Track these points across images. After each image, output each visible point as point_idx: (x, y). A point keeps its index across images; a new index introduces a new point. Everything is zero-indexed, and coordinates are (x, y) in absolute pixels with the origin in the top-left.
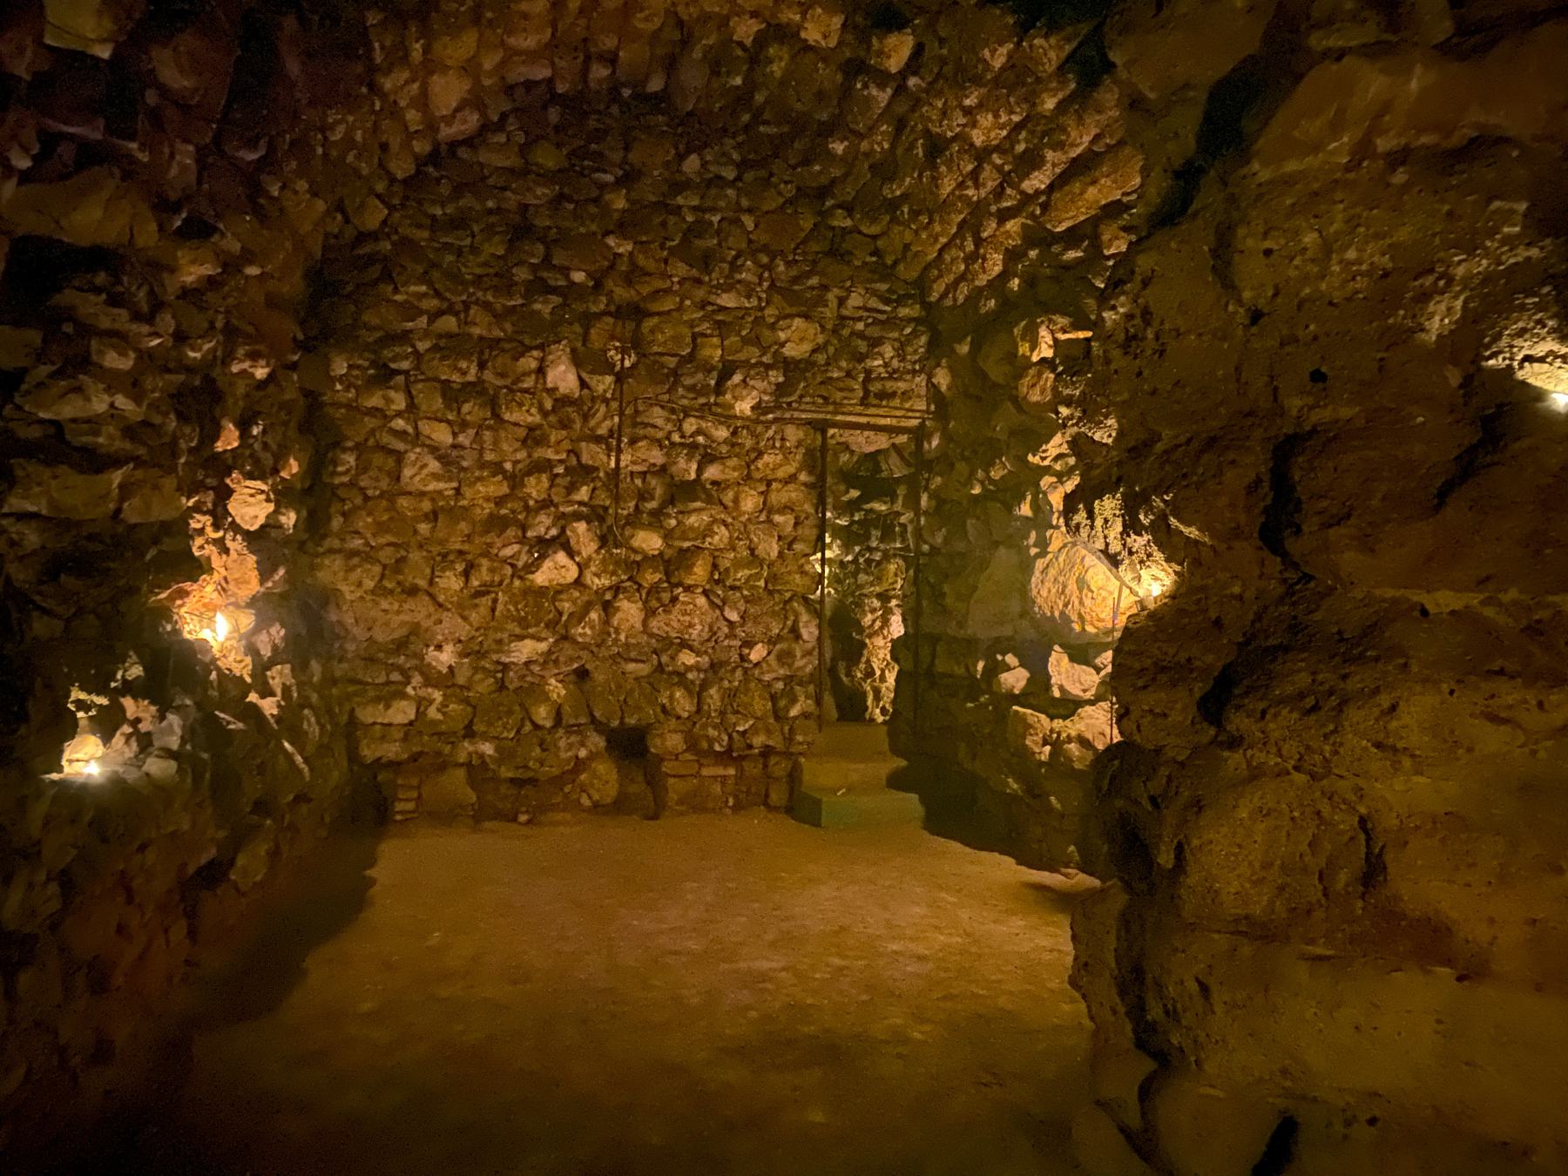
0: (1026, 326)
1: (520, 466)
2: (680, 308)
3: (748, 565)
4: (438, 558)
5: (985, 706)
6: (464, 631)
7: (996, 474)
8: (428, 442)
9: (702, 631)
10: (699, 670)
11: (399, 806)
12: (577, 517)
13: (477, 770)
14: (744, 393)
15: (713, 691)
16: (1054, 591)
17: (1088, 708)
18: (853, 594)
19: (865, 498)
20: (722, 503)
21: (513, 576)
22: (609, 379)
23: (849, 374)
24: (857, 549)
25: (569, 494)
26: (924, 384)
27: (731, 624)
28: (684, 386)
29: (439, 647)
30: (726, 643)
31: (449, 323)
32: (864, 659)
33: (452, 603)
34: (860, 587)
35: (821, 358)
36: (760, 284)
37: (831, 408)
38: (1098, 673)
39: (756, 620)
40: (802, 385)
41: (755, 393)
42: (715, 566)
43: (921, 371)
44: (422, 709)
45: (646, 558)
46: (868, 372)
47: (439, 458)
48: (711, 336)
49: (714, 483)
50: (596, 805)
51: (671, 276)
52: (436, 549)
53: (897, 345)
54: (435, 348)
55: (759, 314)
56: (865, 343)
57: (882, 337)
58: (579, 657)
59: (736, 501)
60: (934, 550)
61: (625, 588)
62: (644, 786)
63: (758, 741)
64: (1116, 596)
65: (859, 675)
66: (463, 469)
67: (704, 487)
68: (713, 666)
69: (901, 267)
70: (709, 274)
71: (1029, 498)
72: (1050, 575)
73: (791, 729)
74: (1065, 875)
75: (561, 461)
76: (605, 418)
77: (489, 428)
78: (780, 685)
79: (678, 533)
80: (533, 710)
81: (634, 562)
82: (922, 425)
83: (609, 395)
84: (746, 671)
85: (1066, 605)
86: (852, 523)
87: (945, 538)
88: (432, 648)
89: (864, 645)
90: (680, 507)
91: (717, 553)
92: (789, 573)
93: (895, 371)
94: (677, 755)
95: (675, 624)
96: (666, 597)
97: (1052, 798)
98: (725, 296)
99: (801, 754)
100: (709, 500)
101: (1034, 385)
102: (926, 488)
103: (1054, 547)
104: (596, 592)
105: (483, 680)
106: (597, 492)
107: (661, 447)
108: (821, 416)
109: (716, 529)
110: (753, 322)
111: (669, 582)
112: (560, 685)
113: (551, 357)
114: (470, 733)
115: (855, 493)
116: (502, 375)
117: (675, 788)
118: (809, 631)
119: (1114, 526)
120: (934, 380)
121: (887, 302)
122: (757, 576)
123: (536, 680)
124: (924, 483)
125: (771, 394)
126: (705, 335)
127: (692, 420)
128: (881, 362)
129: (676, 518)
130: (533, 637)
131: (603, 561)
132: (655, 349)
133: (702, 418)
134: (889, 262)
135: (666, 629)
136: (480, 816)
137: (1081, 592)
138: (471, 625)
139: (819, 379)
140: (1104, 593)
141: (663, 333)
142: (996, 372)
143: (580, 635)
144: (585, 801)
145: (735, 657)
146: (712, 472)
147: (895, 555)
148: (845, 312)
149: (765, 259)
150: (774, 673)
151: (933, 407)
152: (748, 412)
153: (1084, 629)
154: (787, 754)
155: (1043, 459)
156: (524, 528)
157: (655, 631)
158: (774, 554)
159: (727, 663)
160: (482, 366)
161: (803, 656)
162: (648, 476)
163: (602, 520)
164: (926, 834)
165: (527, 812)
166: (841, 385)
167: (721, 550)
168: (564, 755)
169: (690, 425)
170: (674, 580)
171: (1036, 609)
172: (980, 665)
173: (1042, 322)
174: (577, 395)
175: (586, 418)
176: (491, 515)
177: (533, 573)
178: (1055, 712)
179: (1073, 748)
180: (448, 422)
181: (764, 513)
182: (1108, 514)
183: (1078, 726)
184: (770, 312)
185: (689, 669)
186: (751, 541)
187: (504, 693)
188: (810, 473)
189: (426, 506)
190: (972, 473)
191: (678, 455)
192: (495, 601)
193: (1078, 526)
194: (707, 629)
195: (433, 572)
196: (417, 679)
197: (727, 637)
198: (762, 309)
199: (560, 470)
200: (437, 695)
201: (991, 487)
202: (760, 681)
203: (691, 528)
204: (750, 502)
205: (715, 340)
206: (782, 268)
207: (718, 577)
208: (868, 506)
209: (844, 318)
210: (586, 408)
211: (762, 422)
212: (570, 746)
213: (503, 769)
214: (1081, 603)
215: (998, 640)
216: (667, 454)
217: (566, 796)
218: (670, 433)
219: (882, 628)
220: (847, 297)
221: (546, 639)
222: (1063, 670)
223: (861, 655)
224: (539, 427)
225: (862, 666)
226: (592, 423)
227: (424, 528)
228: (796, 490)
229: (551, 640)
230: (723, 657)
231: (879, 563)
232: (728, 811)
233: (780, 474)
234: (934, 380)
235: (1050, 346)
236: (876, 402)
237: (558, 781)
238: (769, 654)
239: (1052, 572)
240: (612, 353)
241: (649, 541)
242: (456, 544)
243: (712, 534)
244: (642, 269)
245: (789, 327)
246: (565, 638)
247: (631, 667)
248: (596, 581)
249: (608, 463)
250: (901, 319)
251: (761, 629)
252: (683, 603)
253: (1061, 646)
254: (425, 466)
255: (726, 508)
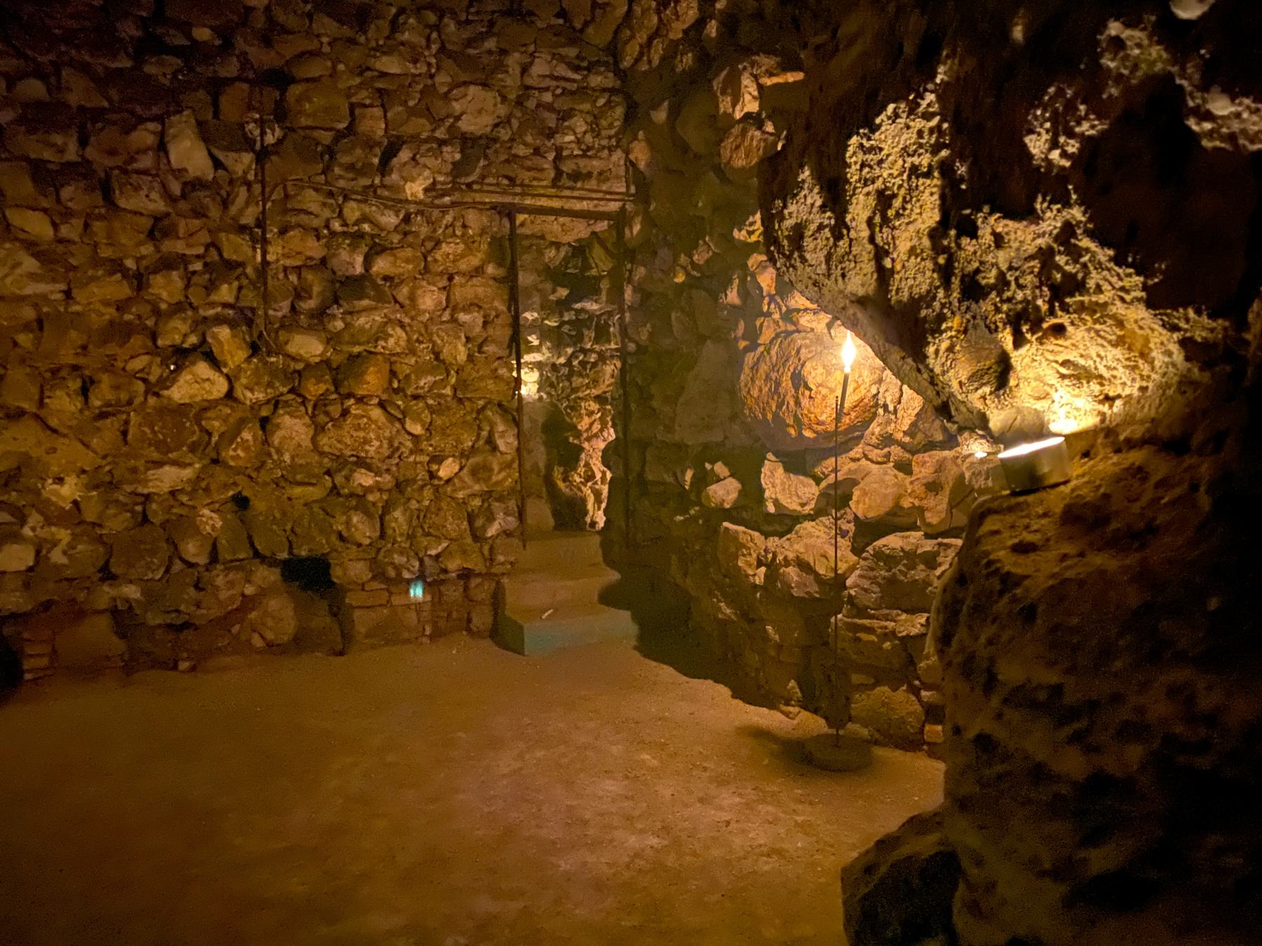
0: (727, 75)
1: (144, 263)
2: (333, 74)
3: (432, 371)
4: (48, 375)
5: (694, 519)
6: (87, 460)
7: (700, 257)
8: (22, 236)
9: (381, 446)
10: (380, 490)
11: (27, 664)
12: (219, 320)
13: (122, 617)
14: (415, 172)
15: (397, 514)
16: (766, 389)
17: (808, 525)
18: (567, 397)
19: (575, 296)
20: (396, 301)
21: (146, 393)
22: (247, 158)
23: (537, 152)
24: (570, 351)
25: (208, 295)
26: (622, 162)
27: (416, 438)
28: (340, 165)
29: (60, 480)
30: (412, 459)
31: (34, 88)
32: (582, 463)
33: (70, 427)
34: (575, 390)
35: (505, 134)
36: (428, 47)
37: (518, 190)
38: (818, 484)
39: (443, 431)
40: (482, 163)
41: (427, 173)
42: (393, 373)
43: (618, 146)
44: (44, 552)
45: (308, 365)
46: (559, 150)
47: (36, 255)
48: (371, 106)
49: (386, 278)
50: (270, 645)
51: (318, 36)
52: (43, 366)
53: (589, 119)
54: (20, 120)
55: (429, 82)
56: (554, 116)
57: (572, 109)
58: (235, 484)
59: (412, 298)
60: (641, 349)
61: (286, 402)
62: (328, 619)
63: (453, 565)
64: (839, 395)
65: (578, 480)
66: (74, 268)
67: (375, 286)
68: (399, 486)
69: (590, 30)
70: (365, 32)
71: (737, 281)
72: (761, 371)
73: (491, 549)
74: (787, 714)
75: (198, 257)
76: (247, 204)
77: (100, 217)
78: (477, 502)
79: (346, 337)
80: (181, 547)
81: (295, 371)
82: (623, 208)
83: (251, 177)
84: (437, 489)
85: (780, 406)
86: (562, 323)
87: (651, 334)
88: (50, 481)
89: (582, 449)
90: (346, 306)
91: (394, 359)
92: (482, 378)
93: (589, 149)
94: (363, 585)
95: (348, 441)
96: (335, 410)
97: (769, 628)
98: (385, 59)
99: (503, 574)
100: (380, 298)
101: (738, 147)
102: (630, 281)
103: (765, 338)
104: (252, 408)
105: (115, 516)
106: (244, 292)
107: (318, 238)
108: (508, 199)
109: (390, 331)
110: (422, 92)
111: (339, 394)
112: (214, 515)
113: (172, 131)
114: (107, 575)
115: (563, 292)
116: (112, 153)
117: (362, 621)
118: (508, 442)
119: (913, 210)
120: (632, 157)
121: (577, 69)
122: (443, 383)
123: (183, 511)
124: (627, 274)
125: (446, 174)
126: (366, 106)
127: (353, 204)
128: (571, 138)
129: (343, 319)
130: (175, 463)
131: (256, 372)
132: (304, 121)
133: (365, 201)
134: (578, 26)
135: (339, 446)
136: (130, 667)
137: (797, 390)
138: (95, 452)
139: (503, 158)
140: (824, 391)
141: (310, 102)
142: (694, 136)
143: (233, 458)
144: (257, 642)
145: (422, 475)
146: (382, 265)
147: (612, 357)
148: (529, 82)
149: (432, 18)
150: (470, 488)
151: (633, 190)
152: (421, 196)
153: (800, 434)
154: (488, 575)
155: (750, 233)
156: (154, 337)
157: (326, 449)
158: (462, 356)
159: (414, 481)
160: (83, 142)
161: (500, 471)
162: (303, 270)
163: (250, 323)
164: (637, 654)
165: (188, 658)
166: (529, 163)
167: (398, 354)
168: (224, 595)
169: (352, 211)
170: (343, 391)
171: (747, 412)
172: (689, 475)
173: (745, 68)
174: (210, 177)
175: (225, 204)
176: (111, 323)
177: (168, 388)
178: (770, 528)
179: (792, 572)
180: (45, 211)
181: (448, 312)
182: (890, 174)
183: (796, 547)
184: (442, 79)
185: (369, 490)
186: (434, 343)
187: (147, 528)
188: (500, 264)
189: (29, 313)
190: (676, 259)
191: (339, 246)
192: (127, 422)
193: (798, 234)
194: (386, 446)
195: (42, 392)
196: (35, 518)
197: (411, 452)
198: (432, 76)
199: (198, 266)
200: (64, 535)
201: (695, 273)
202: (453, 498)
203: (362, 329)
204: (429, 299)
205: (377, 112)
206: (452, 27)
207: (396, 384)
208: (578, 306)
209: (528, 88)
210: (224, 193)
211: (438, 207)
212: (231, 584)
213: (149, 615)
214: (798, 403)
215: (706, 447)
216: (328, 246)
217: (236, 637)
218: (328, 221)
219: (601, 430)
220: (531, 63)
221: (190, 465)
222: (778, 482)
223: (577, 460)
224: (168, 215)
225: (581, 470)
226: (233, 210)
227: (24, 339)
228: (484, 285)
229: (197, 466)
230: (410, 474)
231: (594, 365)
232: (425, 640)
233: (463, 266)
234: (632, 157)
235: (754, 98)
236: (570, 184)
237: (224, 621)
238: (461, 469)
239: (763, 368)
240: (252, 126)
241: (309, 347)
242: (67, 356)
243: (387, 337)
244: (282, 26)
245: (466, 95)
246: (215, 461)
247: (298, 491)
248: (249, 394)
249: (254, 257)
250: (594, 90)
251: (451, 441)
252: (356, 416)
253: (774, 454)
254: (19, 264)
255: (402, 306)
